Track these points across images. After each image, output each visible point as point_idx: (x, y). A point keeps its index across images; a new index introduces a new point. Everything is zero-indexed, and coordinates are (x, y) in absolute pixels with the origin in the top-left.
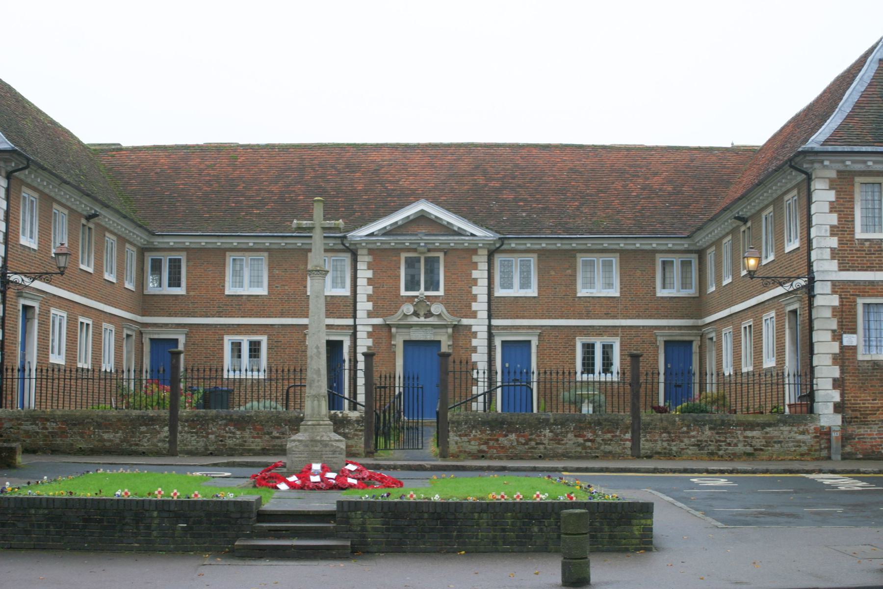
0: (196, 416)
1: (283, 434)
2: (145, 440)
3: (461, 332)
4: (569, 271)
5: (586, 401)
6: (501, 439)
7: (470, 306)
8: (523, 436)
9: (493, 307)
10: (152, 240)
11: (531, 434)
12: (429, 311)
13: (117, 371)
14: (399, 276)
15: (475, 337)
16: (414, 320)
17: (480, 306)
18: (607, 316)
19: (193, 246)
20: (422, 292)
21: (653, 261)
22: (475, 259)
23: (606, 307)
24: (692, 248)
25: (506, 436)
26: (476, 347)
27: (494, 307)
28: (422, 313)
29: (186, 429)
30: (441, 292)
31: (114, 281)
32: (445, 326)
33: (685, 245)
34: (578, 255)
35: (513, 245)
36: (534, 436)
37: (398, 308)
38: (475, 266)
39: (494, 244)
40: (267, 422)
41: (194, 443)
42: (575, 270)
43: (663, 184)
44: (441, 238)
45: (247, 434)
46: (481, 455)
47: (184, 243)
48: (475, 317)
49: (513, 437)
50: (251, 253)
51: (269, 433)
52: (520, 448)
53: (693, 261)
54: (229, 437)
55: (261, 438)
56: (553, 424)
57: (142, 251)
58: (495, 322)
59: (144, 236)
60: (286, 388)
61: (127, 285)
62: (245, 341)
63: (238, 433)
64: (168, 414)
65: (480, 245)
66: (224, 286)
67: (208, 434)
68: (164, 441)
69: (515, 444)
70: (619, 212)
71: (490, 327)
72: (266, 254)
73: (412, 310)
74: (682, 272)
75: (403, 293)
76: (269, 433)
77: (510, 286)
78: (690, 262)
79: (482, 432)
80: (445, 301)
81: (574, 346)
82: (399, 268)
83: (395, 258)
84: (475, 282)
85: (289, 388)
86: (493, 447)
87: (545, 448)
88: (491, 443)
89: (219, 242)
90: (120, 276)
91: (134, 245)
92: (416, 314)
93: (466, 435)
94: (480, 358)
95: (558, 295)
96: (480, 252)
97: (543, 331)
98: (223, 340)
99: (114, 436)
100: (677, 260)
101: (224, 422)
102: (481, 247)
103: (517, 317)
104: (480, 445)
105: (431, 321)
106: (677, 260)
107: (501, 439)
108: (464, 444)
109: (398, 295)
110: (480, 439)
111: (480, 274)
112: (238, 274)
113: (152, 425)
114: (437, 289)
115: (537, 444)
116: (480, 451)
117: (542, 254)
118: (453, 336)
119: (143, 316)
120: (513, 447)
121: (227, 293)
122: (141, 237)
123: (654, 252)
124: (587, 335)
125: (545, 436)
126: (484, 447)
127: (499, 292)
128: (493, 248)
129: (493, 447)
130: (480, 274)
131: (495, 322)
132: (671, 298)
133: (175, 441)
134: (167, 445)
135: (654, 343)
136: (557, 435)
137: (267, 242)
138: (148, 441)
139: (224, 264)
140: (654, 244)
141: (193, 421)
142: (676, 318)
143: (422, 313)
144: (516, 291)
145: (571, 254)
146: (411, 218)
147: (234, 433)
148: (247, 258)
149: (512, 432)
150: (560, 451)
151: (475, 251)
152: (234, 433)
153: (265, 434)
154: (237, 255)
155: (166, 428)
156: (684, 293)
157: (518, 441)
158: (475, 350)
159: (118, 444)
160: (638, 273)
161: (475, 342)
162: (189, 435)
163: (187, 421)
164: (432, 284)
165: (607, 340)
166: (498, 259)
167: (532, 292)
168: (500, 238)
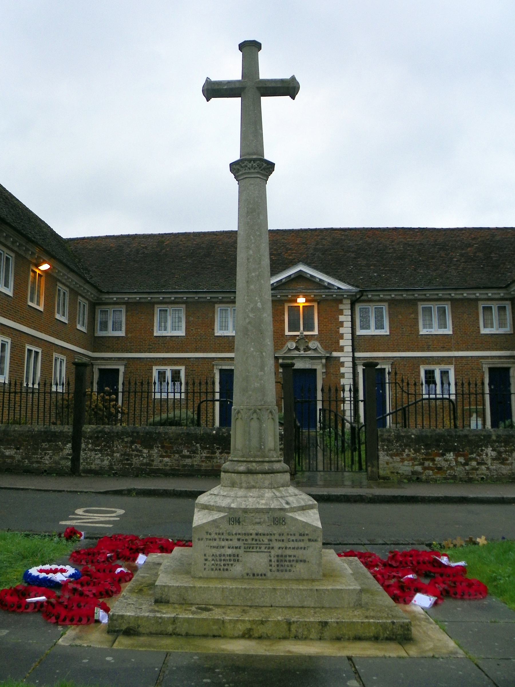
0: (100, 432)
1: (194, 452)
2: (47, 457)
3: (332, 363)
4: (413, 316)
5: (474, 415)
6: (437, 459)
7: (338, 343)
8: (461, 455)
9: (356, 343)
10: (101, 297)
11: (472, 453)
12: (307, 347)
13: (10, 384)
14: (284, 320)
15: (343, 366)
16: (296, 353)
17: (346, 342)
18: (443, 349)
19: (130, 301)
20: (301, 332)
21: (477, 308)
22: (341, 307)
23: (442, 343)
24: (507, 296)
25: (443, 455)
26: (343, 374)
27: (357, 343)
28: (302, 348)
29: (90, 446)
30: (316, 332)
31: (67, 322)
32: (320, 358)
33: (502, 293)
34: (419, 303)
35: (370, 296)
36: (474, 456)
37: (283, 345)
38: (341, 312)
39: (355, 295)
40: (177, 439)
41: (98, 462)
42: (417, 314)
43: (476, 253)
44: (315, 291)
45: (155, 451)
46: (415, 479)
47: (124, 298)
48: (343, 351)
49: (451, 456)
50: (173, 306)
51: (179, 452)
52: (460, 468)
53: (507, 306)
54: (136, 456)
55: (169, 457)
56: (495, 441)
57: (93, 306)
58: (357, 355)
59: (93, 292)
60: (197, 402)
61: (79, 327)
62: (168, 370)
63: (145, 451)
64: (71, 430)
65: (345, 296)
66: (153, 330)
67: (113, 452)
68: (68, 458)
69: (454, 463)
70: (446, 272)
71: (354, 358)
72: (184, 306)
73: (294, 345)
74: (499, 315)
75: (287, 333)
76: (179, 452)
77: (368, 328)
78: (505, 307)
79: (417, 451)
80: (319, 338)
81: (419, 372)
82: (284, 314)
83: (280, 307)
84: (341, 324)
85: (201, 402)
86: (429, 468)
87: (488, 469)
88: (427, 463)
89: (149, 297)
90: (72, 317)
91: (87, 299)
92: (297, 349)
93: (397, 455)
94: (347, 382)
95: (405, 334)
96: (345, 301)
97: (394, 361)
98: (152, 369)
99: (16, 453)
100: (495, 306)
101: (130, 439)
102: (345, 298)
103: (374, 351)
104: (413, 465)
105: (310, 353)
106: (495, 306)
107: (437, 459)
108: (396, 465)
109: (283, 334)
110: (414, 459)
111: (345, 318)
112: (163, 320)
113: (55, 441)
114: (312, 329)
115: (478, 464)
116: (414, 473)
117: (392, 303)
118: (326, 366)
119: (94, 352)
120: (451, 468)
121: (155, 334)
122: (92, 293)
123: (477, 300)
124: (429, 364)
125: (487, 455)
126: (419, 468)
127: (360, 332)
128: (354, 298)
129: (429, 468)
130: (345, 318)
131: (357, 355)
132: (492, 335)
133: (78, 460)
134: (69, 463)
135: (480, 369)
136: (500, 453)
137: (185, 296)
138: (51, 458)
139: (153, 315)
140: (478, 294)
141: (97, 437)
142: (497, 350)
143: (302, 348)
144: (372, 331)
145: (414, 303)
146: (292, 276)
147: (141, 451)
148: (170, 308)
149: (450, 451)
150: (504, 472)
151: (341, 301)
152: (141, 451)
153: (174, 453)
154: (163, 307)
155: (69, 445)
156: (501, 331)
157: (456, 461)
158: (343, 376)
159: (19, 461)
160: (465, 316)
161: (342, 370)
162: (93, 453)
163: (91, 438)
164: (309, 326)
165: (444, 367)
166: (358, 307)
167: (385, 331)
168: (360, 291)
